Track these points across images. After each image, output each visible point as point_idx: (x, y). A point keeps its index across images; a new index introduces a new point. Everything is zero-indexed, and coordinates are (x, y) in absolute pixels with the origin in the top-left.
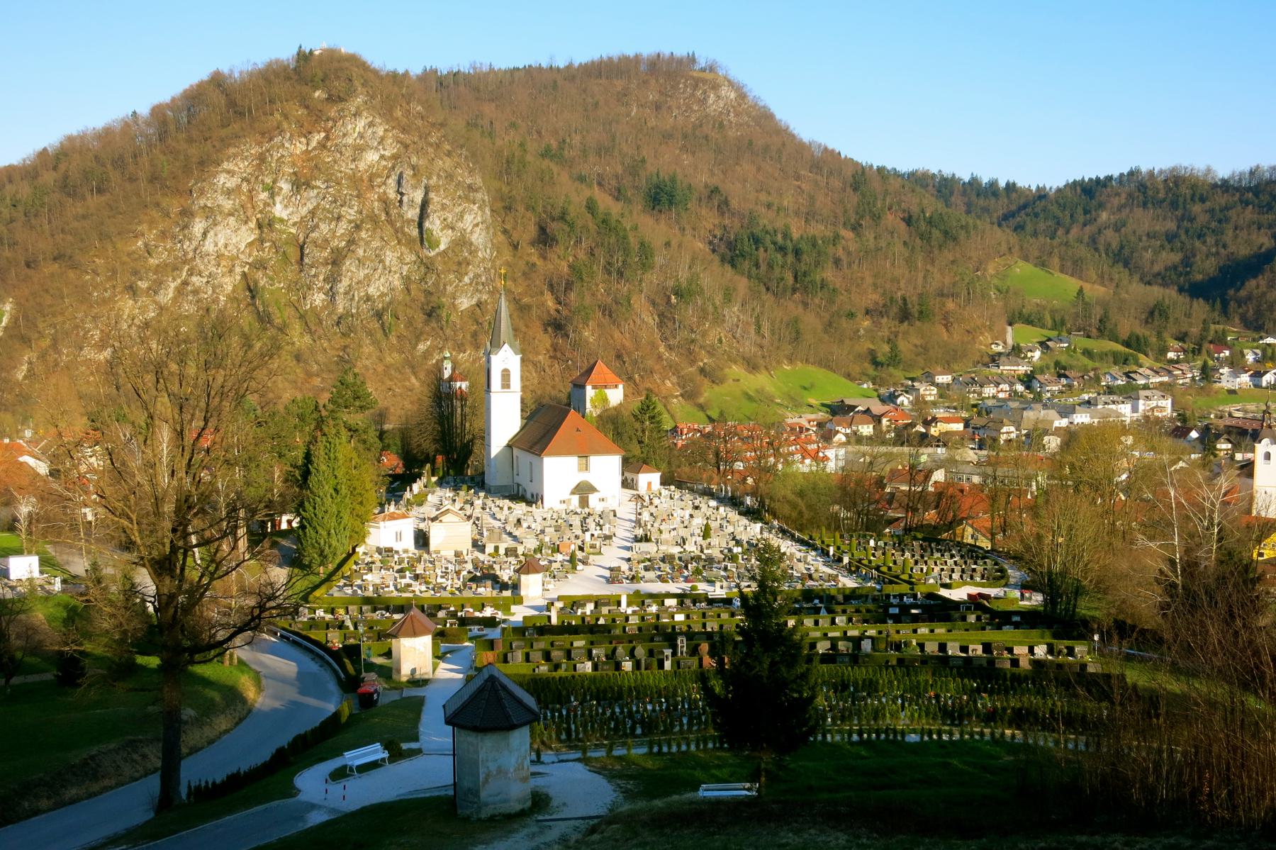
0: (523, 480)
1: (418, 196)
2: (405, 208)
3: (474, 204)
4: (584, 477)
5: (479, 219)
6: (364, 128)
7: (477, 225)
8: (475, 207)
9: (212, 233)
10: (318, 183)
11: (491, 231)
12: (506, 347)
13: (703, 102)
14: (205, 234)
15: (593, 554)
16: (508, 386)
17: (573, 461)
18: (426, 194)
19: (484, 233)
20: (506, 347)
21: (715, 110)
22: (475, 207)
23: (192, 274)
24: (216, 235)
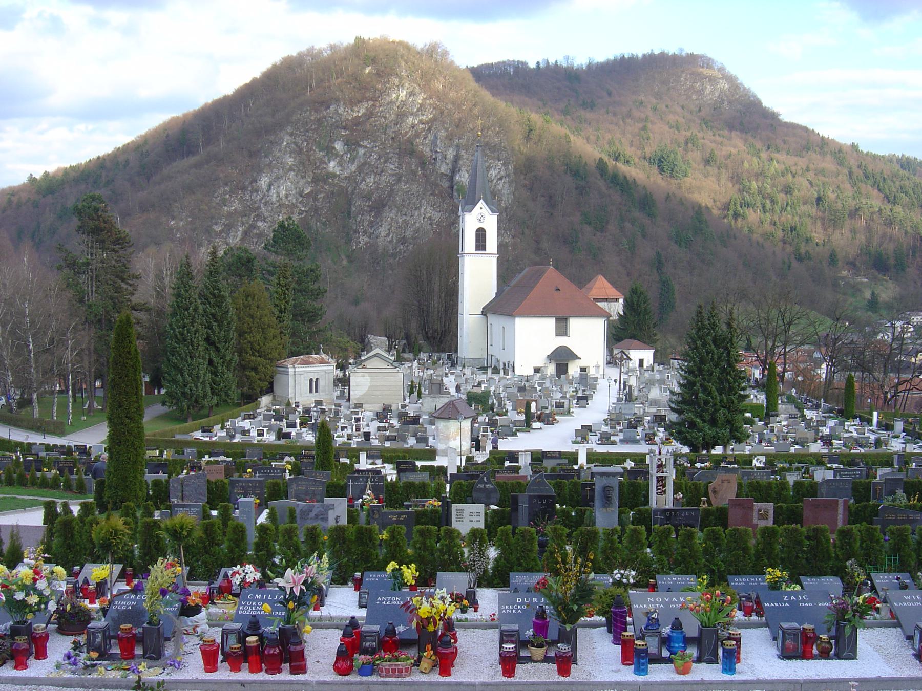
0: (495, 351)
1: (451, 153)
2: (438, 164)
3: (499, 160)
4: (562, 341)
5: (503, 173)
6: (406, 96)
7: (501, 179)
8: (500, 164)
9: (276, 185)
10: (365, 143)
11: (514, 185)
12: (481, 203)
13: (701, 92)
14: (270, 186)
15: (513, 371)
16: (484, 248)
17: (549, 324)
18: (458, 151)
19: (507, 185)
20: (481, 203)
21: (711, 99)
22: (500, 164)
23: (257, 220)
24: (279, 187)
